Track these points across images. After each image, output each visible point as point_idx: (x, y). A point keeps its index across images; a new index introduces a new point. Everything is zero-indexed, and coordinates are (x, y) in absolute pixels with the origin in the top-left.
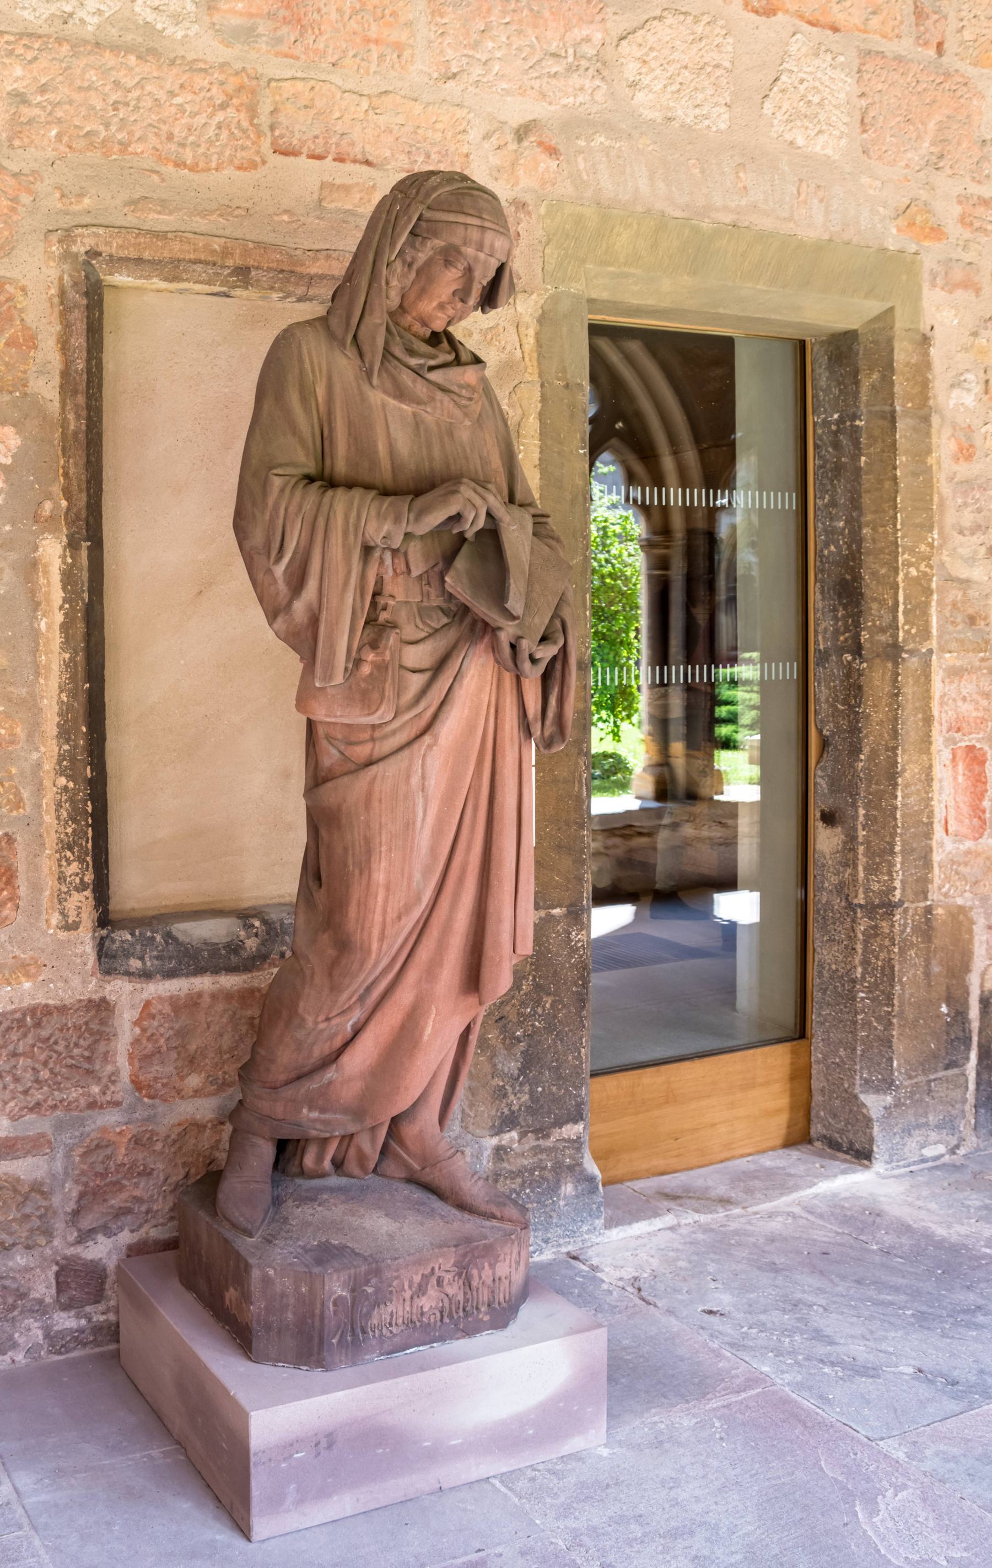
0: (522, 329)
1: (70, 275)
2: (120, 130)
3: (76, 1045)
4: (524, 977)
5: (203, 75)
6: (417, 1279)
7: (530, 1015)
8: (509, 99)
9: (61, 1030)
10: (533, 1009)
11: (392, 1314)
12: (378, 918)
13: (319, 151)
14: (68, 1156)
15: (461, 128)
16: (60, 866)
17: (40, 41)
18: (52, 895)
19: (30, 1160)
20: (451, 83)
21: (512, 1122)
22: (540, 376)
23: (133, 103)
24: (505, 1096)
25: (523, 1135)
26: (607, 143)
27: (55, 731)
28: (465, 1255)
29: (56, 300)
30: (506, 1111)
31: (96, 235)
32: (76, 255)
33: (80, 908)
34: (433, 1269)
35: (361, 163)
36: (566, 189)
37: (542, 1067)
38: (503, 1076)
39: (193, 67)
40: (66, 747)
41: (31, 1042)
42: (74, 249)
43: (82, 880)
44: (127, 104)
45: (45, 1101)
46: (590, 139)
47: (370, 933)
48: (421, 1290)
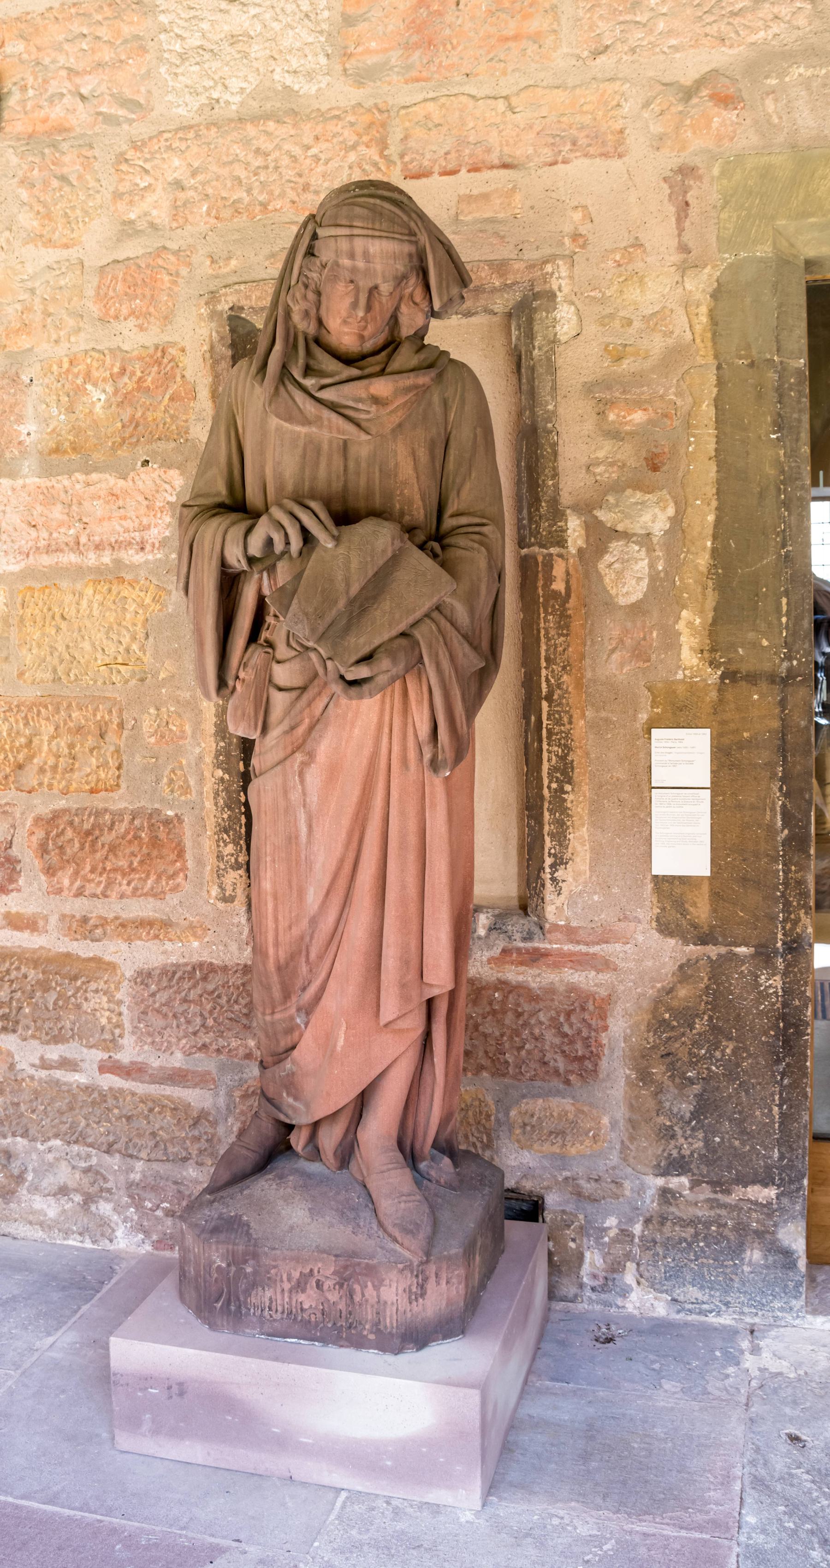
1: (217, 332)
2: (261, 192)
3: (236, 1002)
4: (697, 1015)
5: (335, 121)
6: (296, 1275)
7: (704, 1057)
8: (678, 55)
9: (223, 987)
11: (271, 1299)
12: (271, 924)
13: (450, 167)
14: (230, 1095)
15: (614, 103)
16: (218, 846)
17: (192, 131)
18: (212, 870)
19: (197, 1091)
20: (603, 58)
21: (681, 1167)
22: (716, 357)
23: (272, 165)
24: (673, 1137)
26: (809, 73)
27: (213, 730)
28: (346, 1267)
29: (208, 355)
30: (675, 1153)
31: (238, 292)
32: (221, 313)
33: (235, 884)
34: (311, 1270)
35: (498, 167)
36: (748, 139)
37: (720, 1116)
38: (671, 1115)
39: (324, 117)
40: (222, 744)
41: (199, 992)
42: (219, 308)
43: (236, 860)
45: (211, 1044)
46: (781, 75)
47: (266, 937)
48: (300, 1286)
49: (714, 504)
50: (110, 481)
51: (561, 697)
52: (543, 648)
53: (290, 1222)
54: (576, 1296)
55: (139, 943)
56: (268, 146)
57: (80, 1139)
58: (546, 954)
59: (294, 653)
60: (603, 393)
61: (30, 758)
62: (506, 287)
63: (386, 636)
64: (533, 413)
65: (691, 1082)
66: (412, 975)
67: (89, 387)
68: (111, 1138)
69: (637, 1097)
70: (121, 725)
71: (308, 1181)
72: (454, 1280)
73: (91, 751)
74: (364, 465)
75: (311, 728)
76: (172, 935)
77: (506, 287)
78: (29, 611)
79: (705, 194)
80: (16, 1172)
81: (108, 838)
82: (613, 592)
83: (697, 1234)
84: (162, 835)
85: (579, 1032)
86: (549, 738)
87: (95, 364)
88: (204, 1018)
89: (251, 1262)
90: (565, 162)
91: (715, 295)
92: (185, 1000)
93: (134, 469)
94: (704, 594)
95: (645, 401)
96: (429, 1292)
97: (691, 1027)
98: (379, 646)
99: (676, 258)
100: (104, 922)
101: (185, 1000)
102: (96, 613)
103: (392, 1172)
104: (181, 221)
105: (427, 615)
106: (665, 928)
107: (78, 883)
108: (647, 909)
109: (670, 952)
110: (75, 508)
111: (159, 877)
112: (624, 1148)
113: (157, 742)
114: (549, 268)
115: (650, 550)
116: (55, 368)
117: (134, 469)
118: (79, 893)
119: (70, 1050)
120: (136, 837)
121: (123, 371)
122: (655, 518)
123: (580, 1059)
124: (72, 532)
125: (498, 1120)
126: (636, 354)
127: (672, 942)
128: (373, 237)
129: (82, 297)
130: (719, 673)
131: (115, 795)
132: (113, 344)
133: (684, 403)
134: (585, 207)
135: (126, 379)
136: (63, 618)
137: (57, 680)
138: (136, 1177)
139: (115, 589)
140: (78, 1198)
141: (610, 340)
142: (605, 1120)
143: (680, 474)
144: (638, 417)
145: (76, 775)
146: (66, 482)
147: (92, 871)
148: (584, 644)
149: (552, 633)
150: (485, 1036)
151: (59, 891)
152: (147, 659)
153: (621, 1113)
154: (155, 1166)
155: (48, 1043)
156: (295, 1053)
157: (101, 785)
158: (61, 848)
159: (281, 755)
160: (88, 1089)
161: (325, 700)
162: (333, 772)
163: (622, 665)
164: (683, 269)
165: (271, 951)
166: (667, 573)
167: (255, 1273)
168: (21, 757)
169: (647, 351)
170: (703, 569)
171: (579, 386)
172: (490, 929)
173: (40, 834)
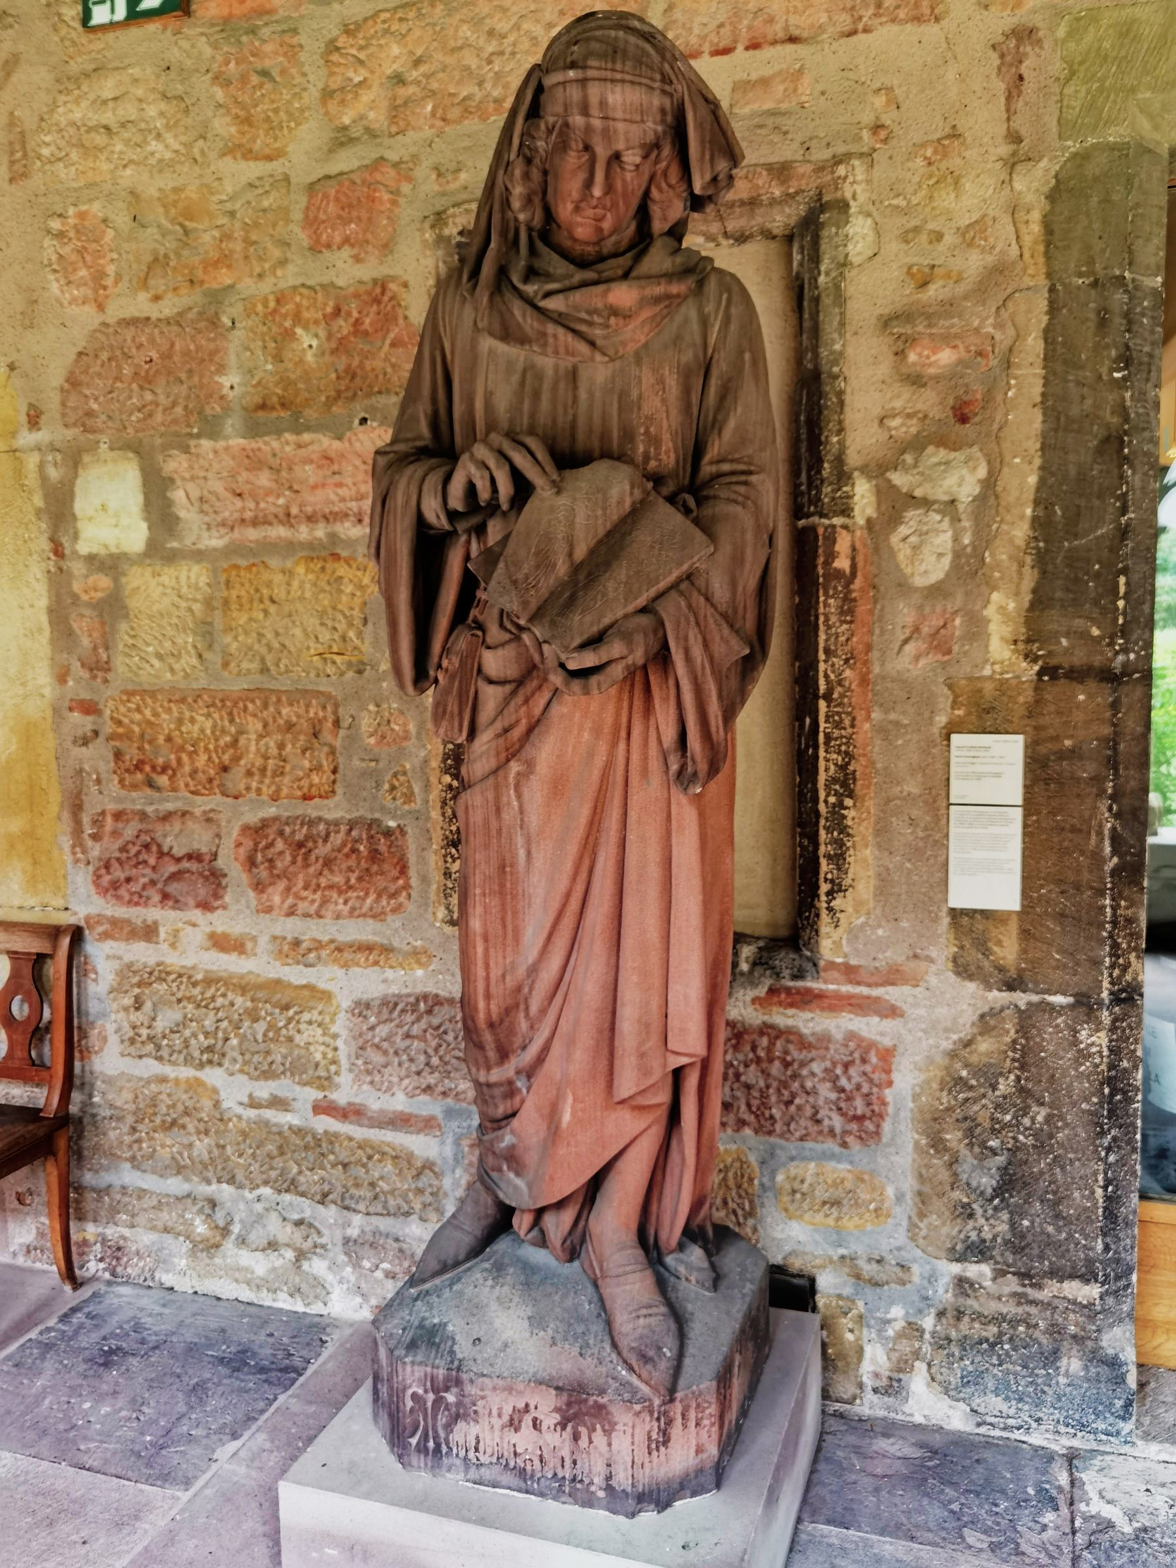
0: (1021, 215)
6: (508, 1410)
7: (1008, 1125)
10: (1015, 1117)
19: (421, 1137)
22: (1049, 275)
24: (971, 1216)
25: (999, 1274)
30: (974, 1236)
32: (449, 238)
42: (446, 232)
44: (502, 53)
48: (514, 1424)
49: (1038, 462)
50: (325, 442)
51: (842, 696)
52: (822, 637)
53: (504, 1337)
54: (854, 1398)
55: (357, 970)
56: (503, 26)
57: (292, 1186)
58: (820, 996)
59: (507, 636)
60: (901, 327)
61: (236, 759)
62: (789, 197)
63: (620, 613)
64: (816, 355)
65: (994, 1152)
66: (654, 1041)
67: (299, 331)
68: (326, 1188)
69: (928, 1166)
70: (337, 723)
71: (531, 1280)
72: (706, 1422)
73: (304, 752)
74: (598, 395)
75: (530, 731)
76: (393, 962)
77: (789, 197)
78: (234, 594)
79: (1044, 64)
80: (221, 1224)
81: (323, 850)
82: (908, 571)
83: (1001, 1334)
84: (382, 846)
85: (858, 1087)
86: (827, 743)
87: (305, 303)
88: (428, 1056)
89: (454, 1390)
90: (866, 30)
91: (1053, 196)
92: (408, 1036)
93: (350, 429)
94: (1020, 573)
95: (956, 336)
96: (673, 1438)
97: (994, 1088)
98: (611, 626)
99: (1005, 150)
100: (319, 945)
101: (408, 1036)
102: (308, 595)
103: (631, 1277)
104: (402, 124)
105: (674, 586)
106: (963, 970)
107: (290, 901)
108: (942, 949)
109: (968, 1000)
110: (284, 474)
111: (379, 896)
112: (912, 1227)
113: (379, 743)
114: (841, 170)
115: (956, 520)
116: (260, 308)
117: (350, 429)
118: (291, 913)
119: (282, 1087)
120: (354, 850)
121: (337, 312)
122: (962, 480)
123: (859, 1119)
124: (281, 501)
125: (762, 1185)
126: (948, 276)
127: (971, 987)
128: (613, 81)
129: (288, 221)
130: (1036, 668)
131: (330, 802)
132: (325, 280)
133: (1003, 338)
134: (889, 89)
135: (341, 322)
136: (273, 601)
137: (264, 670)
138: (353, 1232)
139: (329, 566)
140: (290, 1255)
141: (915, 260)
142: (890, 1191)
143: (996, 426)
144: (946, 357)
145: (286, 780)
146: (275, 444)
147: (306, 888)
148: (871, 632)
149: (833, 619)
150: (748, 1087)
151: (269, 910)
152: (366, 647)
153: (909, 1184)
154: (375, 1220)
155: (257, 1079)
156: (515, 1122)
157: (314, 791)
158: (271, 861)
159: (493, 763)
160: (299, 1132)
161: (546, 695)
162: (558, 787)
163: (917, 658)
164: (1012, 164)
165: (481, 1005)
166: (975, 548)
167: (459, 1404)
168: (226, 758)
169: (960, 273)
170: (1020, 542)
171: (873, 321)
172: (754, 964)
173: (248, 844)
